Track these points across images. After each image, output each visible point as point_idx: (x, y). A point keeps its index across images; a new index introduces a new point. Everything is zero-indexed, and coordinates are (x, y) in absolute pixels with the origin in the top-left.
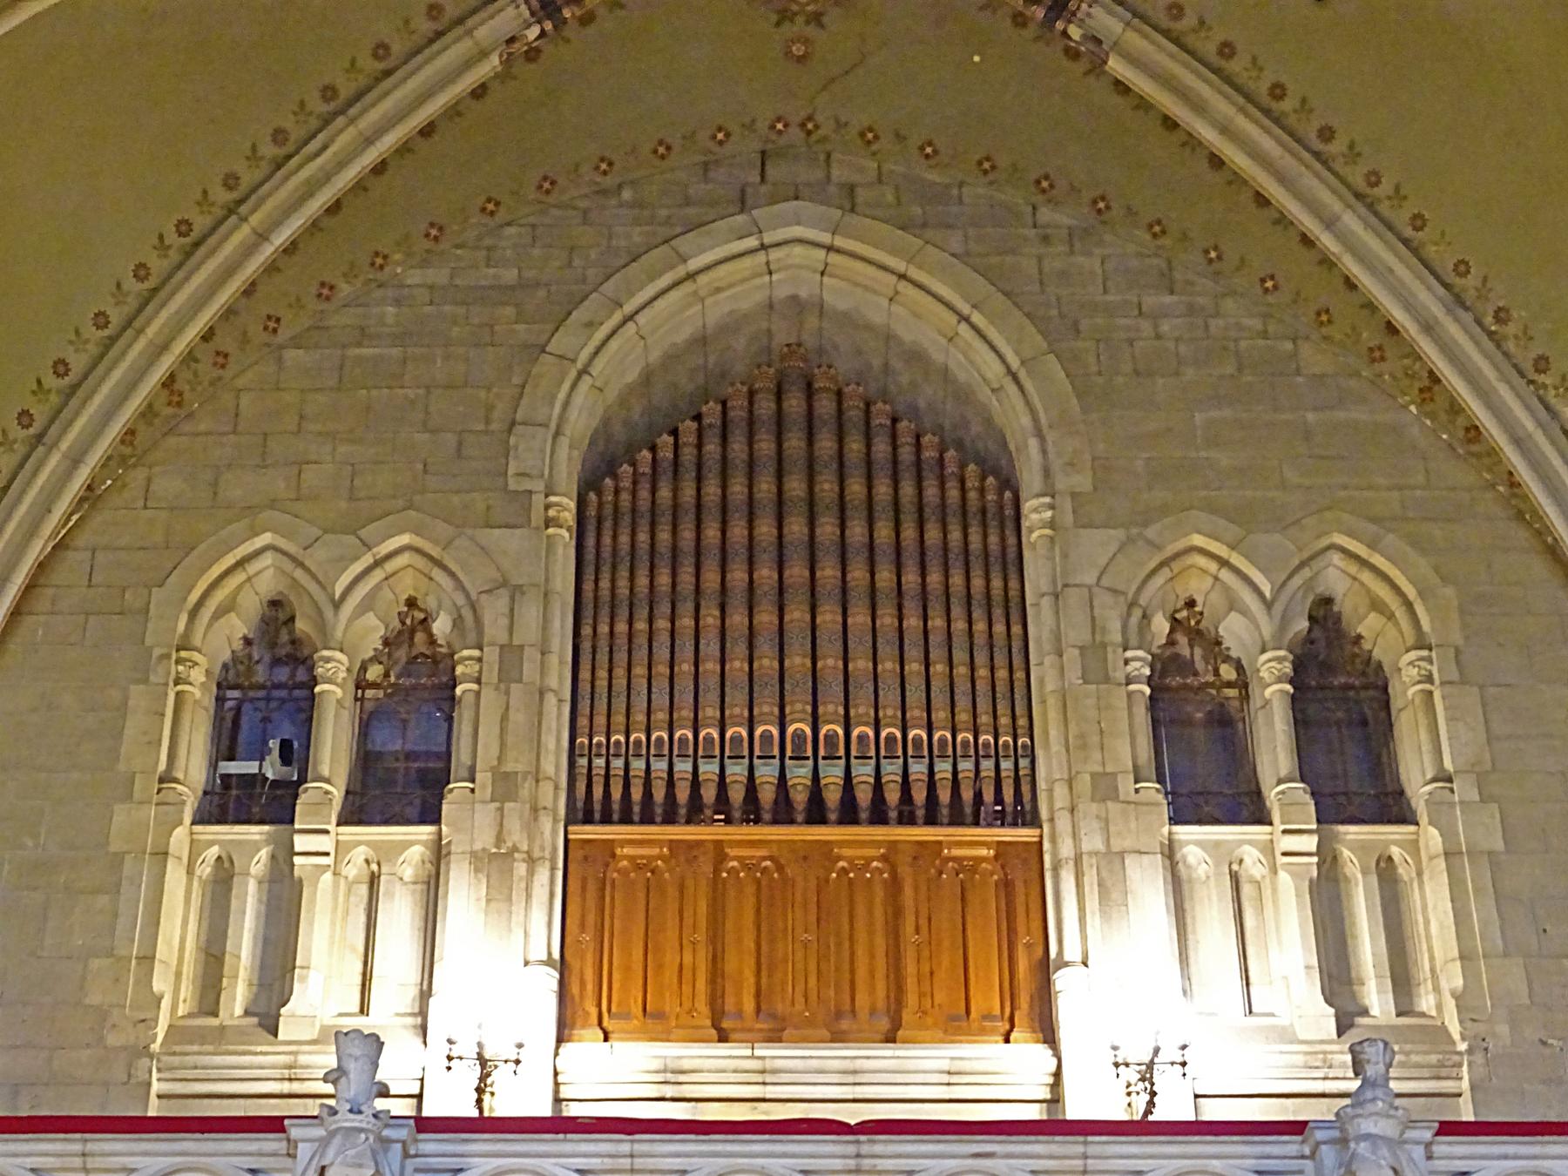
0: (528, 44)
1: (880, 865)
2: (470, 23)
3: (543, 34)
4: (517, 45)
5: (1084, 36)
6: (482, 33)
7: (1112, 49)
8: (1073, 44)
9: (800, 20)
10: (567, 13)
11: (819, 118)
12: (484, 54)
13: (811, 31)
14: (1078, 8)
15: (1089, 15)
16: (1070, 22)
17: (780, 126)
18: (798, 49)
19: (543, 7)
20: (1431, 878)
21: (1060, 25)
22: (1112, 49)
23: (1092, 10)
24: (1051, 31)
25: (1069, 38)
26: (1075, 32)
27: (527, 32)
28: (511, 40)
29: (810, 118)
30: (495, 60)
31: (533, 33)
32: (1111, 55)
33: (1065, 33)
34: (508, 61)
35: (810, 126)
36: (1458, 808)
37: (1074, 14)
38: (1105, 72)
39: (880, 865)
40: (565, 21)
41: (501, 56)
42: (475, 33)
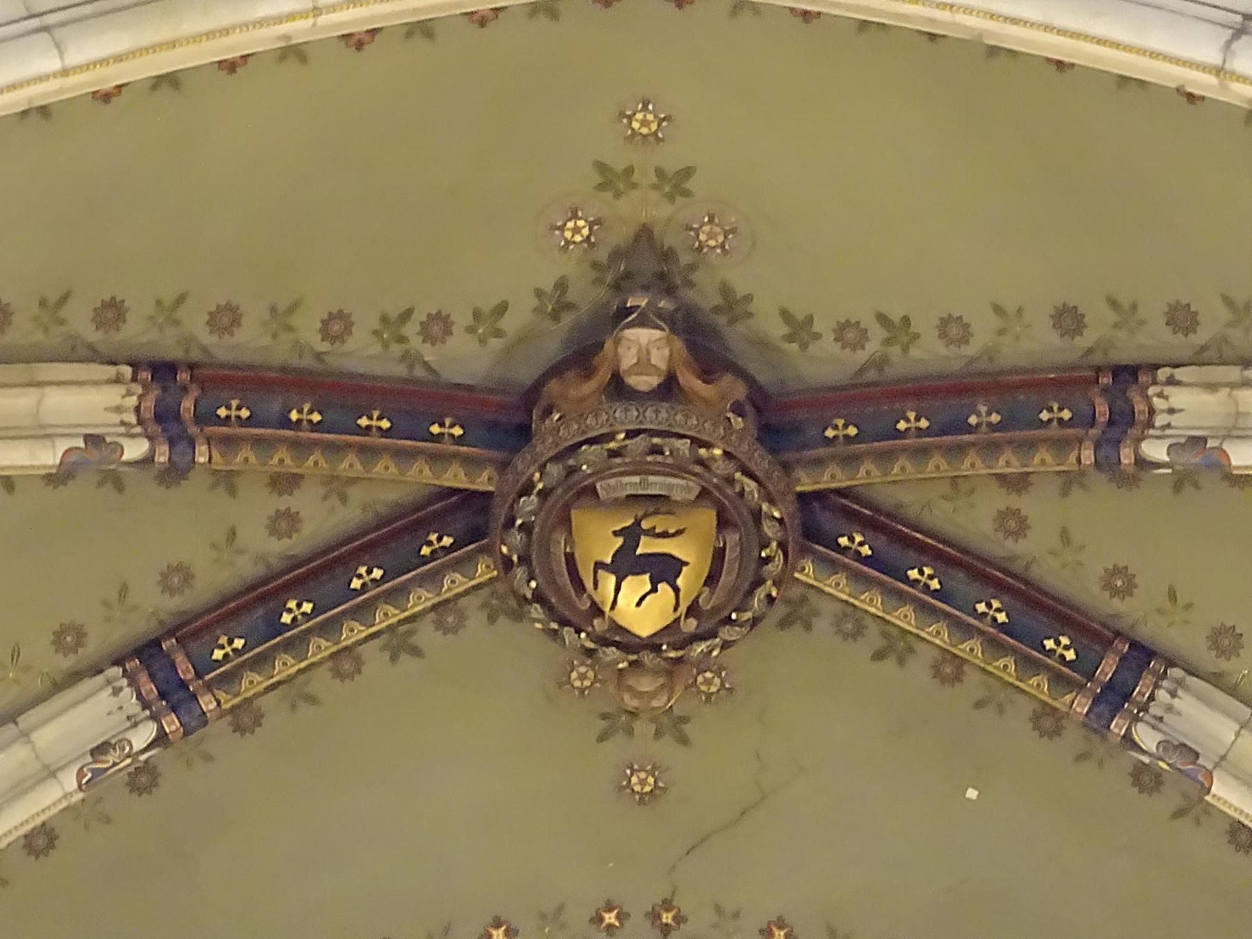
0: (133, 756)
1: (126, 751)
2: (26, 720)
3: (161, 739)
4: (111, 757)
5: (1165, 745)
6: (46, 737)
7: (1216, 765)
8: (1146, 760)
9: (643, 728)
10: (207, 703)
11: (685, 902)
12: (50, 773)
13: (665, 749)
14: (1152, 698)
15: (1170, 709)
16: (1136, 719)
17: (610, 918)
18: (643, 782)
19: (162, 695)
20: (642, 439)
21: (1118, 726)
22: (1216, 765)
23: (1176, 702)
24: (1104, 738)
25: (1135, 746)
26: (1147, 737)
27: (130, 735)
28: (100, 750)
29: (667, 905)
30: (69, 781)
31: (143, 736)
32: (1216, 775)
33: (1128, 740)
34: (92, 782)
35: (667, 918)
36: (608, 281)
37: (1144, 708)
38: (1209, 809)
39: (126, 751)
40: (203, 719)
41: (80, 774)
42: (35, 736)
